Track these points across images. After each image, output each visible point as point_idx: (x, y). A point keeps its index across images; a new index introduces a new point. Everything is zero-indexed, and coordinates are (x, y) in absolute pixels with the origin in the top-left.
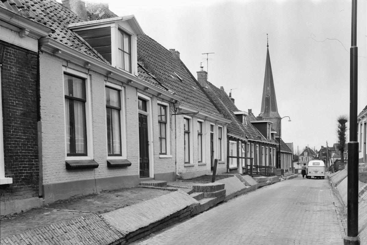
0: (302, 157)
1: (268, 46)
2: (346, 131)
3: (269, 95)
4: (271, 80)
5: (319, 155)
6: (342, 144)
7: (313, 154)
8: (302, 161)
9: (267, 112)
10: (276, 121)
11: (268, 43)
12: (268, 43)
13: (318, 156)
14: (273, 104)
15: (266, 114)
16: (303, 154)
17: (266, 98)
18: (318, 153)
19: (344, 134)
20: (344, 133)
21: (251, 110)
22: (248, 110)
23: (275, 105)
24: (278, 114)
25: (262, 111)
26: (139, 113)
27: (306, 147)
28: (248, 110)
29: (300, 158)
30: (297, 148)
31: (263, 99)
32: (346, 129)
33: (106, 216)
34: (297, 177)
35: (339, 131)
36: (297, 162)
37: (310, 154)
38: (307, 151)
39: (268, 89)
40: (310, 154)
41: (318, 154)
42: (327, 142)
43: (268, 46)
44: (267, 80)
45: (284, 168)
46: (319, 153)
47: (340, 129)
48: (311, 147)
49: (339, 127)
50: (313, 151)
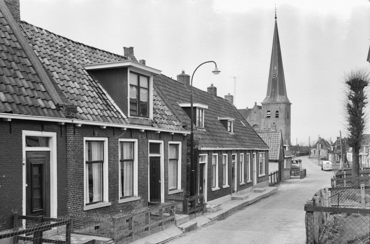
0: (314, 150)
1: (276, 18)
2: (366, 105)
3: (276, 76)
4: (279, 58)
5: (334, 148)
6: (356, 133)
7: (328, 147)
8: (315, 154)
9: (274, 96)
10: (284, 107)
11: (276, 15)
12: (276, 15)
13: (332, 150)
14: (281, 86)
15: (273, 98)
16: (315, 147)
17: (273, 79)
18: (333, 146)
19: (361, 111)
20: (360, 109)
21: (131, 49)
22: (124, 48)
23: (283, 88)
24: (287, 99)
25: (268, 94)
26: (130, 98)
27: (338, 138)
28: (124, 48)
29: (312, 151)
30: (308, 139)
31: (269, 81)
32: (365, 101)
33: (65, 226)
34: (275, 193)
35: (349, 104)
36: (308, 156)
37: (324, 147)
38: (321, 143)
39: (275, 68)
40: (324, 147)
41: (332, 147)
42: (341, 132)
43: (276, 18)
44: (274, 58)
45: (252, 179)
46: (334, 145)
47: (351, 102)
48: (326, 138)
49: (350, 99)
50: (328, 143)
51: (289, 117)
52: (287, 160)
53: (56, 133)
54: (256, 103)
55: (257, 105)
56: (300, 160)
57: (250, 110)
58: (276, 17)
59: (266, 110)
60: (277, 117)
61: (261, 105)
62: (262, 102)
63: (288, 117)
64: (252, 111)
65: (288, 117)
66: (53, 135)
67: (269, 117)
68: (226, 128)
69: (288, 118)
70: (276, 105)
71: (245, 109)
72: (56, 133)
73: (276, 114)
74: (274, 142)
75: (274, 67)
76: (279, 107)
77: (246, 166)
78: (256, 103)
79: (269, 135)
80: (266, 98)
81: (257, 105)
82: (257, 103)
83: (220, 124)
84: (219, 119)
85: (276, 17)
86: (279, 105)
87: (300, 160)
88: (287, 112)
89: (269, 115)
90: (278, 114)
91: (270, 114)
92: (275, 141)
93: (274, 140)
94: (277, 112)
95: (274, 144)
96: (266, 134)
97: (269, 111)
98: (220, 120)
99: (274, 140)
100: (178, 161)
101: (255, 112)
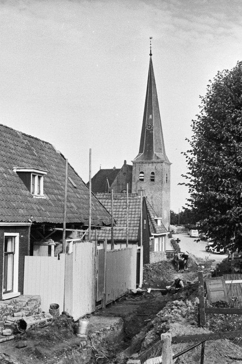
1: (151, 55)
11: (151, 51)
12: (151, 51)
25: (141, 151)
43: (151, 55)
51: (168, 180)
52: (159, 240)
53: (19, 233)
54: (125, 161)
55: (127, 163)
56: (178, 239)
57: (118, 170)
58: (151, 53)
59: (139, 171)
60: (153, 180)
61: (131, 164)
62: (133, 160)
63: (167, 180)
64: (120, 172)
65: (167, 180)
66: (17, 234)
67: (142, 180)
68: (27, 186)
69: (167, 183)
70: (151, 164)
71: (112, 170)
72: (19, 233)
73: (151, 177)
74: (133, 213)
75: (149, 116)
76: (155, 167)
77: (6, 259)
78: (125, 161)
79: (110, 197)
80: (139, 155)
81: (127, 163)
82: (127, 161)
83: (18, 179)
84: (15, 171)
85: (151, 53)
86: (155, 164)
87: (178, 239)
88: (166, 174)
89: (143, 178)
90: (154, 177)
91: (143, 176)
92: (135, 211)
93: (134, 210)
94: (153, 173)
95: (133, 216)
96: (123, 201)
97: (142, 173)
98: (17, 172)
99: (134, 210)
100: (14, 255)
101: (124, 173)
